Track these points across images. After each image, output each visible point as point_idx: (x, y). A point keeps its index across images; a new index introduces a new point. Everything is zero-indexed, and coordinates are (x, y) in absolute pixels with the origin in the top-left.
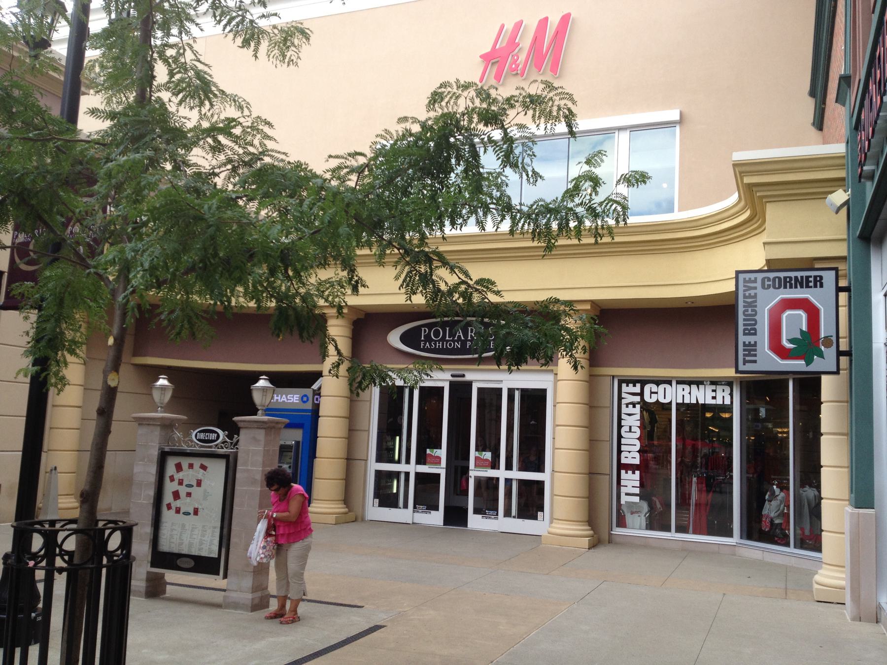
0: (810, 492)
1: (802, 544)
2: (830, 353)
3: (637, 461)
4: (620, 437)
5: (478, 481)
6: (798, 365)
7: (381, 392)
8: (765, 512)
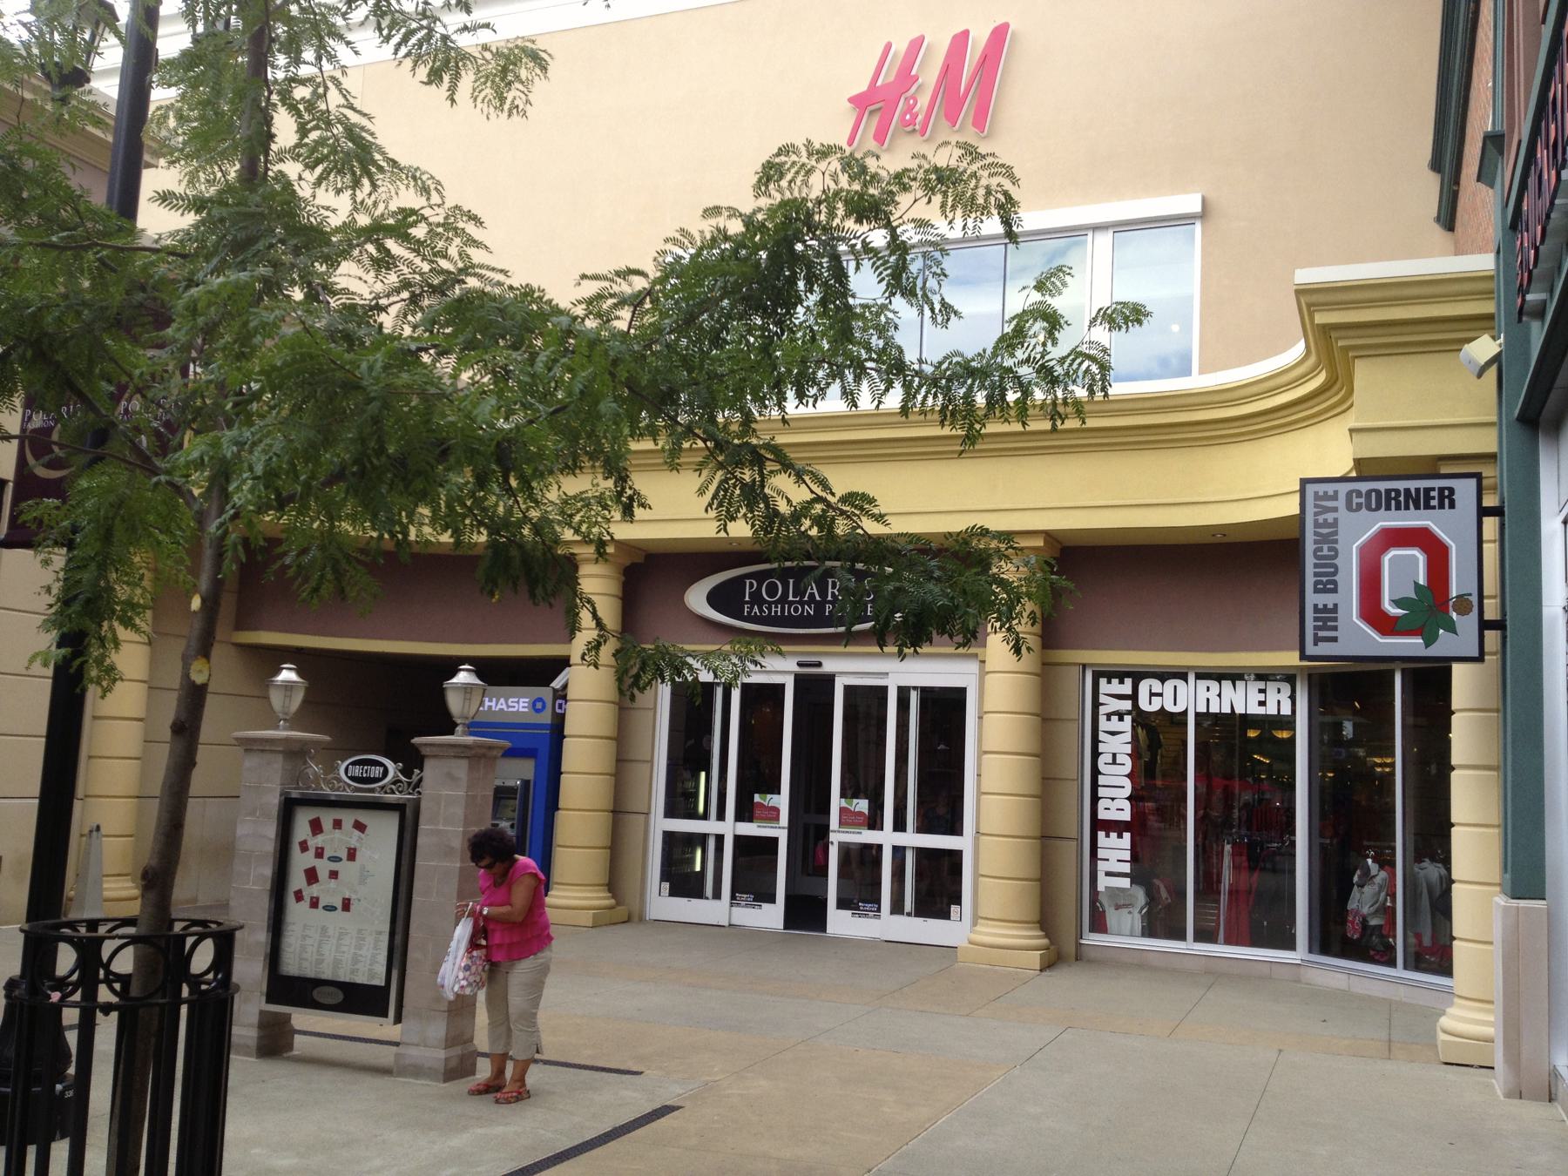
0: (1431, 870)
1: (1418, 961)
3: (1126, 816)
4: (1096, 772)
8: (1352, 905)
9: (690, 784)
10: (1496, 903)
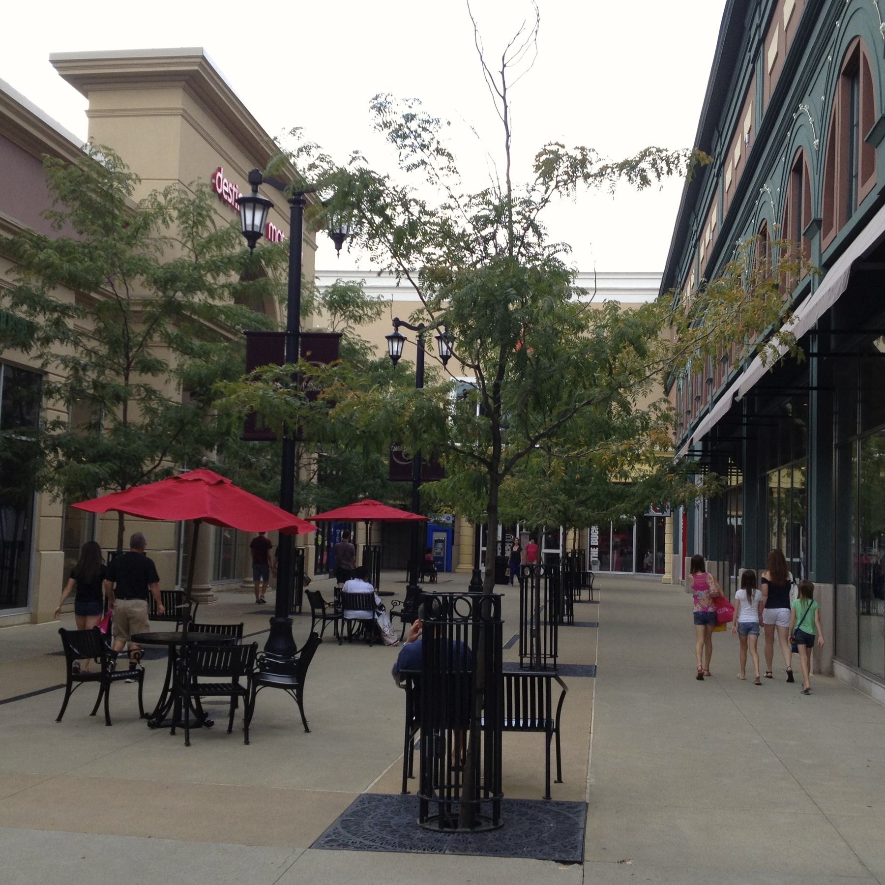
0: (660, 554)
1: (657, 572)
2: (669, 511)
3: (597, 544)
4: (590, 534)
5: (559, 548)
6: (660, 514)
7: (799, 589)
8: (645, 561)
9: (618, 540)
10: (225, 536)
